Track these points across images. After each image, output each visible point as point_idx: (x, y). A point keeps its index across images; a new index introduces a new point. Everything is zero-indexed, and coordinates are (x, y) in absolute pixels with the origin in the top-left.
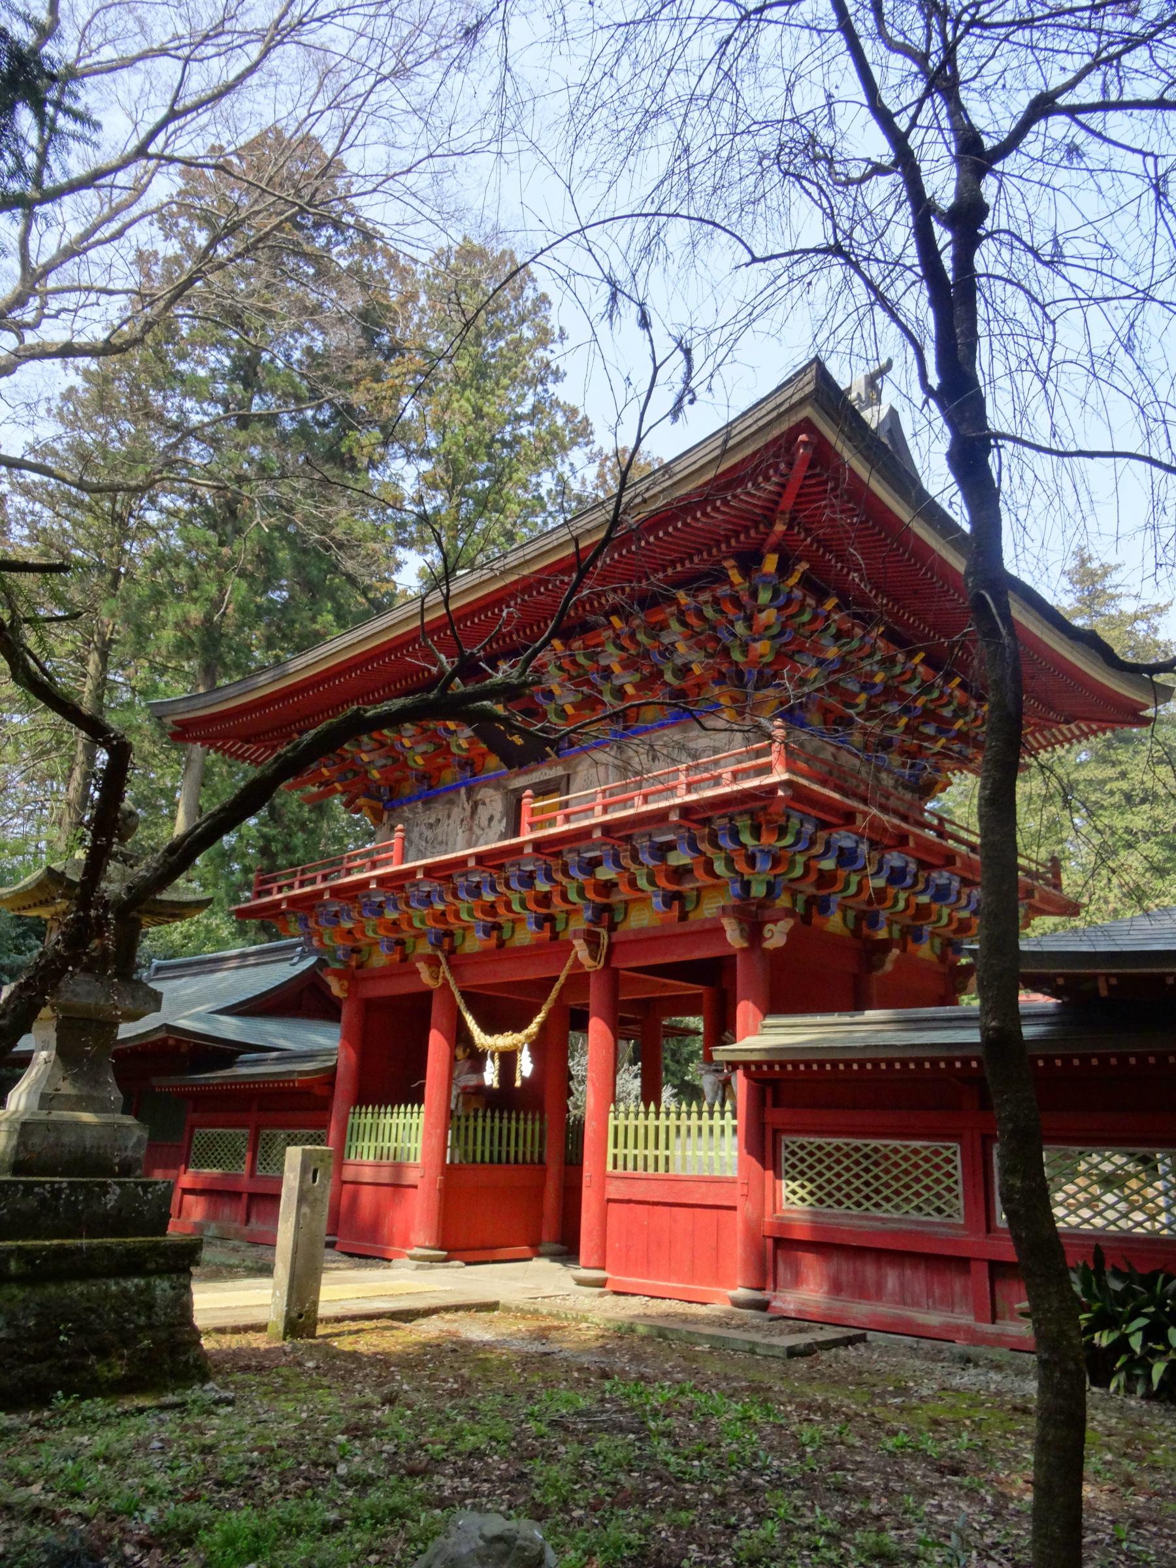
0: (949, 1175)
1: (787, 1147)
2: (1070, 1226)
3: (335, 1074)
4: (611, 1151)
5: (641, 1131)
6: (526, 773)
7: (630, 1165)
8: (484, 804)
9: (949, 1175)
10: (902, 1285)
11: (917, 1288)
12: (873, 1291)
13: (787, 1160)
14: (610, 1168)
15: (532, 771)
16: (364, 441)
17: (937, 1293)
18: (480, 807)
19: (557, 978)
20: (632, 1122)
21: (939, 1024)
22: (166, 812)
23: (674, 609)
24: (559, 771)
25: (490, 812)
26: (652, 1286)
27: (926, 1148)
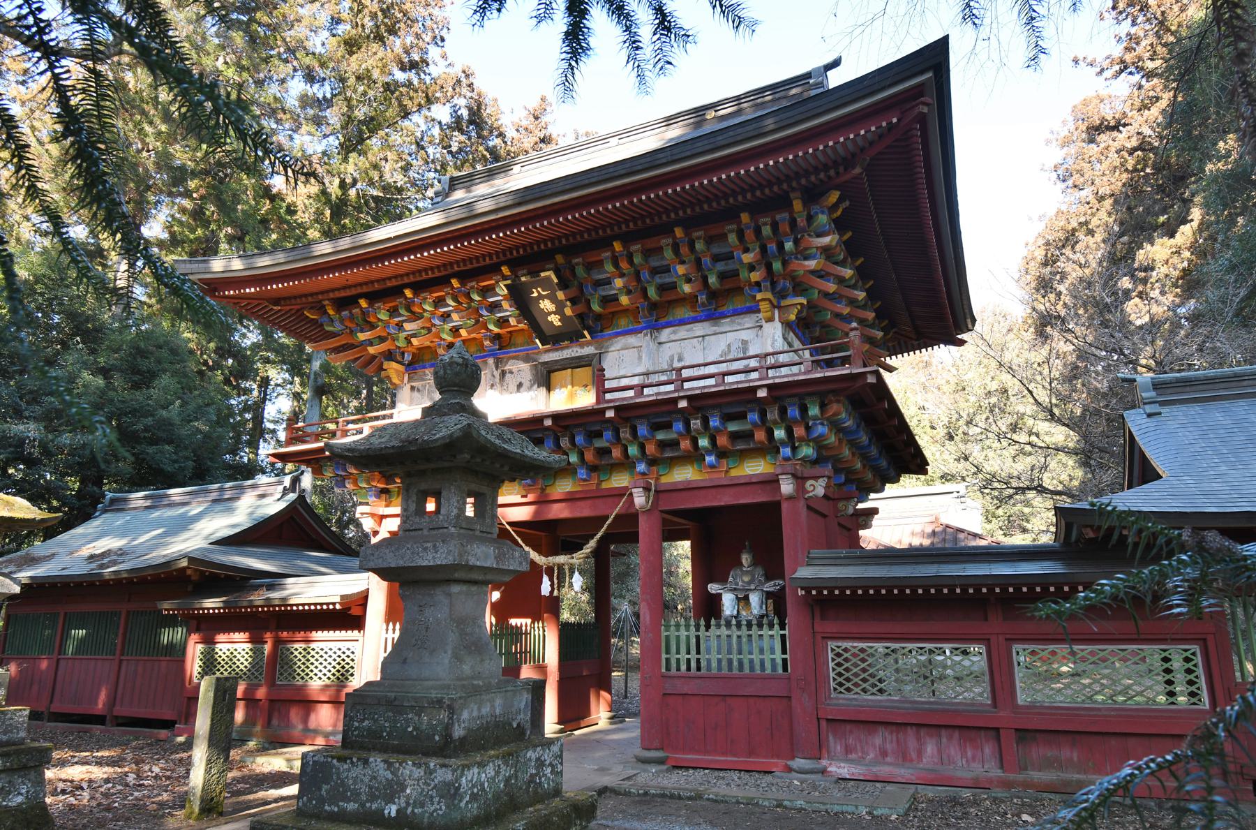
0: (840, 674)
1: (833, 650)
2: (1138, 704)
3: (367, 597)
4: (664, 656)
5: (693, 641)
6: (557, 350)
7: (683, 667)
8: (511, 372)
9: (840, 674)
10: (940, 751)
11: (953, 752)
12: (914, 755)
13: (833, 660)
14: (663, 670)
15: (562, 349)
16: (348, 27)
17: (969, 754)
18: (508, 375)
19: (607, 518)
20: (683, 633)
21: (965, 558)
22: (209, 105)
23: (670, 240)
24: (590, 350)
25: (519, 380)
26: (712, 761)
27: (1082, 650)
